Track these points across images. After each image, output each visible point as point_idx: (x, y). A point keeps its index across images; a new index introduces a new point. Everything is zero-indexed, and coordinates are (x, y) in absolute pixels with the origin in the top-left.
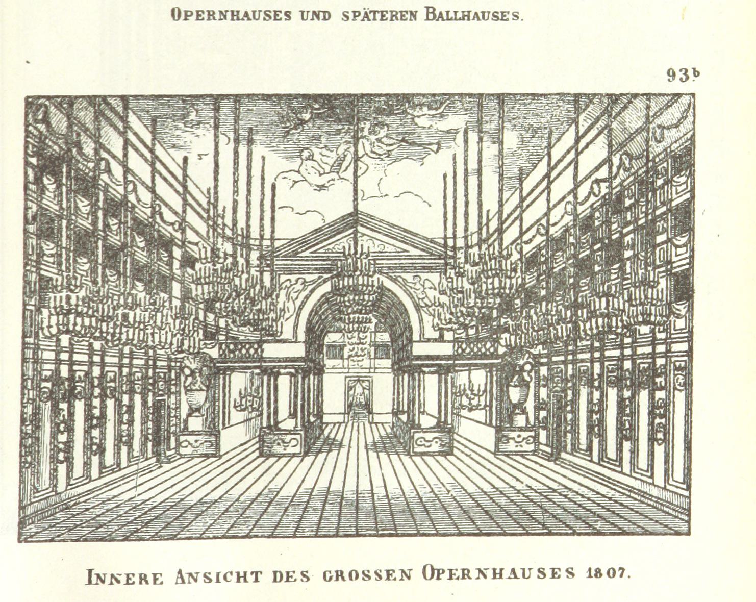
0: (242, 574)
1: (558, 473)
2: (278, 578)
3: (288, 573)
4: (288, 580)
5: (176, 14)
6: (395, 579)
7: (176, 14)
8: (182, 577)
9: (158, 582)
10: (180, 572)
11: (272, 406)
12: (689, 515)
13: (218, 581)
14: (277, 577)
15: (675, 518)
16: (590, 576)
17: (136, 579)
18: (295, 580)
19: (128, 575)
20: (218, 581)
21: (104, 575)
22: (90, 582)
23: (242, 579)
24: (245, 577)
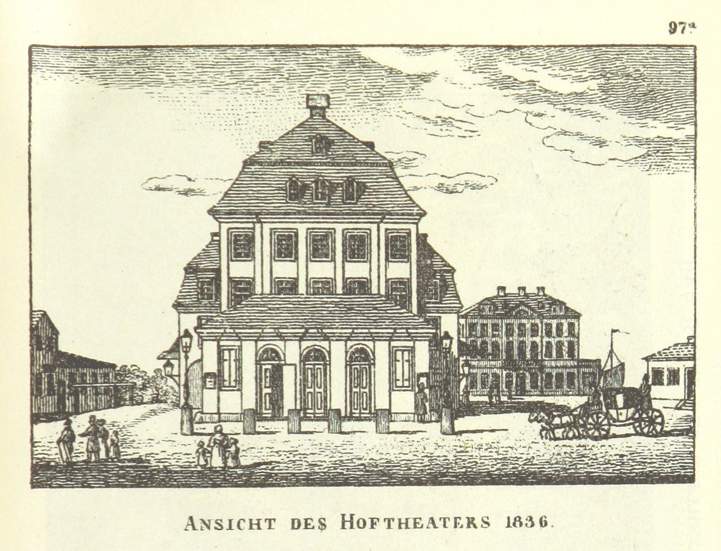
0: (403, 521)
1: (262, 283)
2: (296, 526)
3: (306, 520)
4: (306, 528)
5: (656, 127)
6: (313, 528)
7: (656, 127)
8: (193, 525)
9: (459, 526)
10: (191, 518)
11: (294, 339)
12: (459, 300)
13: (230, 528)
14: (295, 524)
15: (678, 383)
16: (509, 526)
17: (464, 522)
18: (422, 527)
19: (415, 519)
20: (230, 528)
21: (209, 521)
22: (343, 527)
23: (403, 526)
24: (258, 524)
